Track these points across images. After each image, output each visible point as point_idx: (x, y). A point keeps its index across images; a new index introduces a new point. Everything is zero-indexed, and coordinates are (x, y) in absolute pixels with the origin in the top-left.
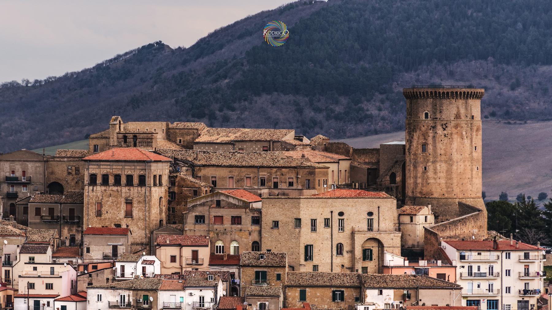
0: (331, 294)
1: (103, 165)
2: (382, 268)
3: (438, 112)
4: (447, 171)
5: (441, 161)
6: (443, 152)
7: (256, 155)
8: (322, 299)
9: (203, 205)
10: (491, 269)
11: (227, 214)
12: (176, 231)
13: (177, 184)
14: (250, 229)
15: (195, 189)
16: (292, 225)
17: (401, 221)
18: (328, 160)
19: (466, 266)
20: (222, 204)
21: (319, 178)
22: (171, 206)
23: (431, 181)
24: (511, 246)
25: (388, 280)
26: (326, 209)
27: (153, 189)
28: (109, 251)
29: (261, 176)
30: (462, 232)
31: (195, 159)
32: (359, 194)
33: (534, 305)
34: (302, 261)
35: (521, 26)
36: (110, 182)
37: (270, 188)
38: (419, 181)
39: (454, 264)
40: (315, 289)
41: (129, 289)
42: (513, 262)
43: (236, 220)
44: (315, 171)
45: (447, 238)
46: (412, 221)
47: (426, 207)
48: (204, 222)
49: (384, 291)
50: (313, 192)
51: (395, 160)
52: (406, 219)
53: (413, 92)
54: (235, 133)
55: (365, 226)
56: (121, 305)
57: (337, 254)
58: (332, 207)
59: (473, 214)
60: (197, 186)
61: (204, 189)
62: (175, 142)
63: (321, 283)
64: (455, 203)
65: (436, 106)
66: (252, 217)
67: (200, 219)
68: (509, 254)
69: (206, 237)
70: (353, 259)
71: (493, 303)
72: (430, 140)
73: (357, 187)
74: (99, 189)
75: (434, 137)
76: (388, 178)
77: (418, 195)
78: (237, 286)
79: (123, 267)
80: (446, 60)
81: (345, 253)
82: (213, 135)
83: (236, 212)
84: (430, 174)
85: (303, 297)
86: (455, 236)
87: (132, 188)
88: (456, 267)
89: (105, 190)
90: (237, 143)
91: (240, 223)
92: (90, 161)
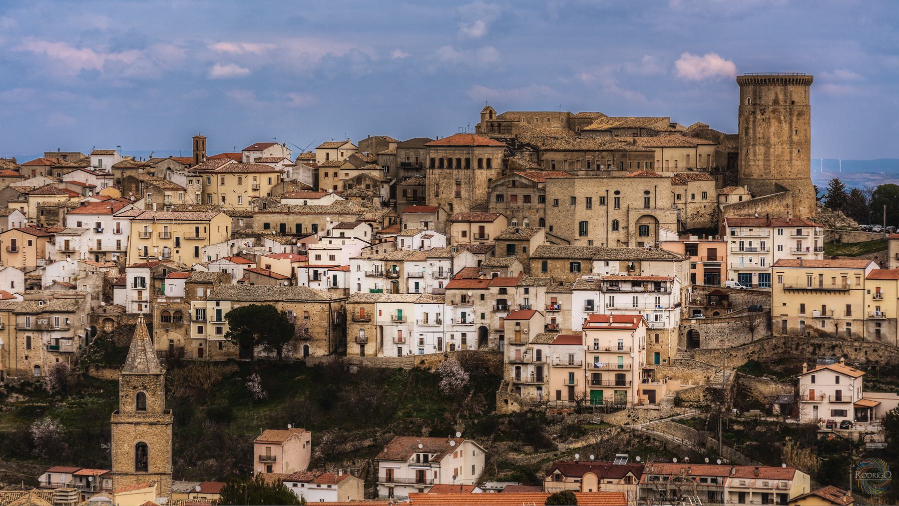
4: (765, 154)
6: (761, 136)
9: (502, 185)
10: (763, 244)
16: (568, 202)
19: (738, 241)
20: (517, 183)
23: (752, 163)
34: (577, 236)
41: (381, 260)
43: (527, 199)
55: (641, 204)
57: (613, 229)
70: (628, 235)
72: (751, 126)
74: (437, 171)
75: (754, 122)
79: (403, 240)
81: (620, 229)
83: (526, 192)
84: (751, 156)
85: (545, 268)
91: (529, 202)
92: (430, 146)
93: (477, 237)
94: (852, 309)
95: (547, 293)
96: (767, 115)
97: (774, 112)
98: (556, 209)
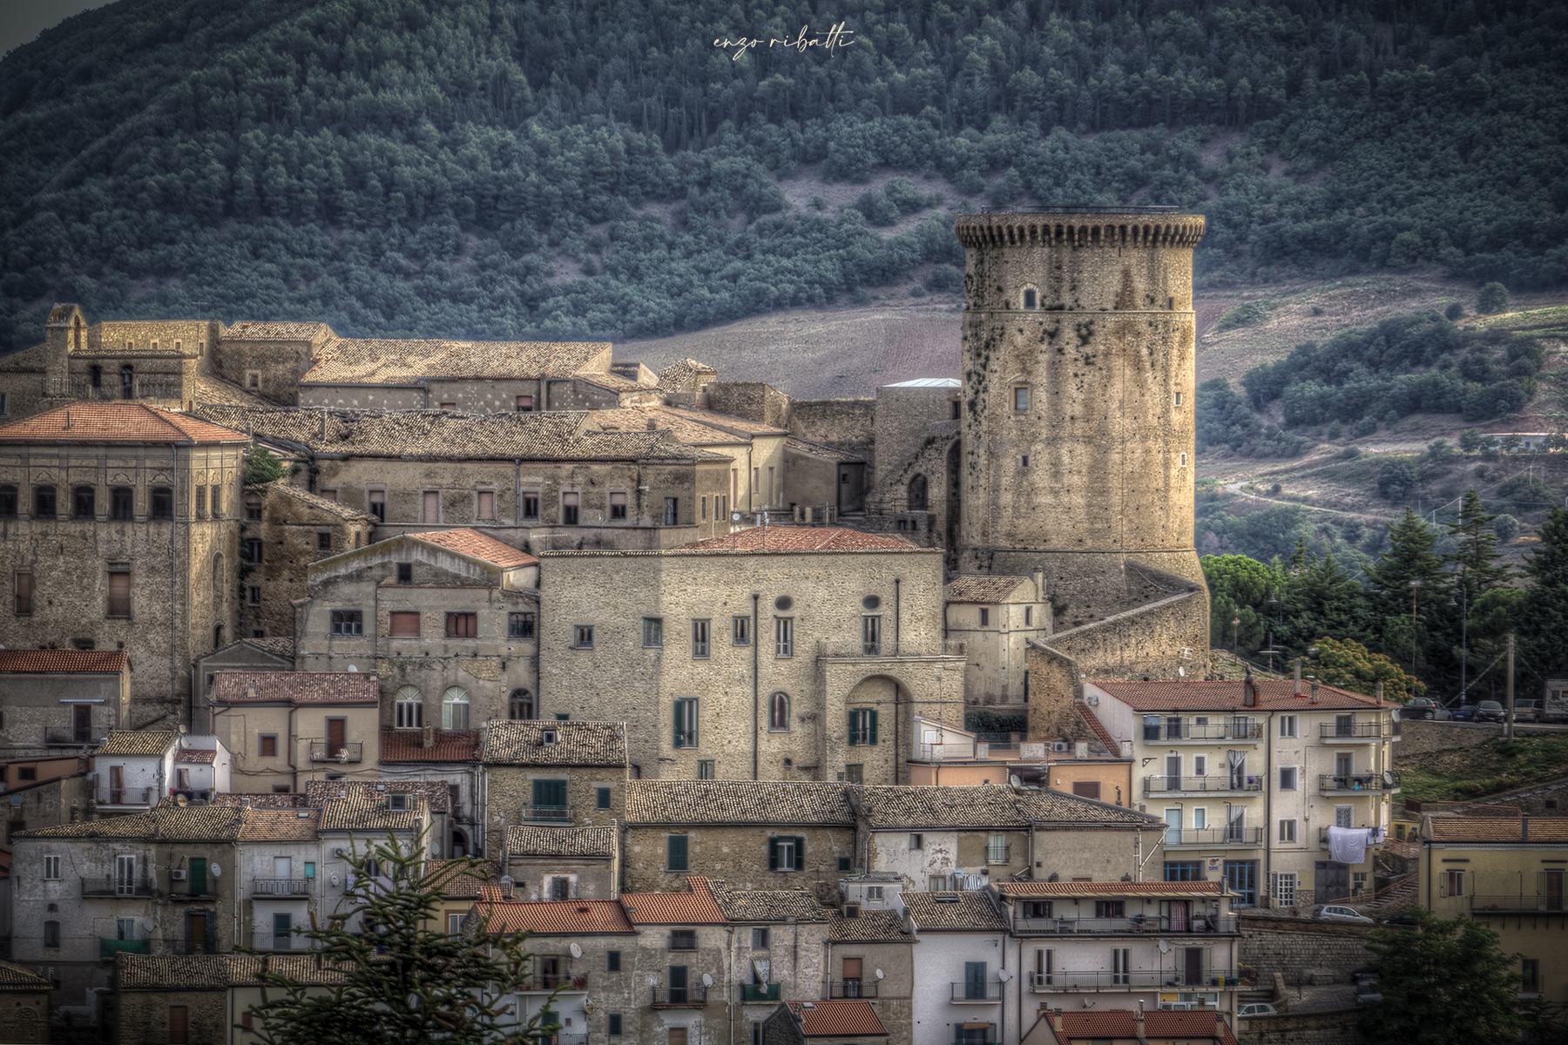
0: (765, 849)
1: (36, 456)
2: (906, 764)
3: (1066, 286)
4: (1092, 469)
5: (1073, 437)
7: (507, 424)
8: (737, 864)
9: (358, 577)
11: (432, 604)
12: (270, 660)
13: (266, 514)
14: (504, 651)
15: (324, 529)
17: (951, 622)
18: (720, 436)
20: (417, 572)
21: (704, 492)
22: (248, 583)
24: (1297, 696)
25: (937, 805)
26: (738, 589)
27: (196, 530)
28: (63, 723)
29: (524, 488)
30: (1142, 654)
31: (315, 435)
32: (836, 541)
33: (1364, 877)
34: (666, 748)
35: (1024, 14)
36: (97, 511)
37: (553, 525)
38: (1007, 498)
39: (1126, 751)
40: (716, 833)
41: (147, 840)
42: (1299, 748)
43: (460, 624)
44: (694, 472)
45: (1096, 674)
46: (985, 620)
47: (1028, 581)
48: (359, 629)
49: (928, 838)
50: (688, 535)
51: (925, 435)
52: (967, 616)
53: (990, 228)
54: (426, 355)
55: (853, 639)
56: (121, 891)
57: (773, 724)
58: (757, 581)
59: (1175, 598)
60: (330, 519)
61: (353, 529)
62: (238, 383)
63: (731, 815)
64: (1116, 566)
65: (1059, 268)
66: (512, 614)
67: (347, 621)
68: (1291, 719)
69: (367, 677)
70: (819, 740)
71: (1241, 870)
72: (1041, 375)
73: (809, 518)
76: (902, 491)
77: (1004, 543)
78: (466, 828)
80: (795, 117)
82: (357, 362)
83: (460, 601)
84: (1041, 477)
86: (1120, 669)
87: (128, 528)
88: (1130, 761)
89: (45, 534)
90: (435, 386)
91: (471, 634)
93: (320, 754)
94: (1542, 971)
95: (830, 943)
96: (1098, 345)
97: (1123, 330)
98: (583, 657)
